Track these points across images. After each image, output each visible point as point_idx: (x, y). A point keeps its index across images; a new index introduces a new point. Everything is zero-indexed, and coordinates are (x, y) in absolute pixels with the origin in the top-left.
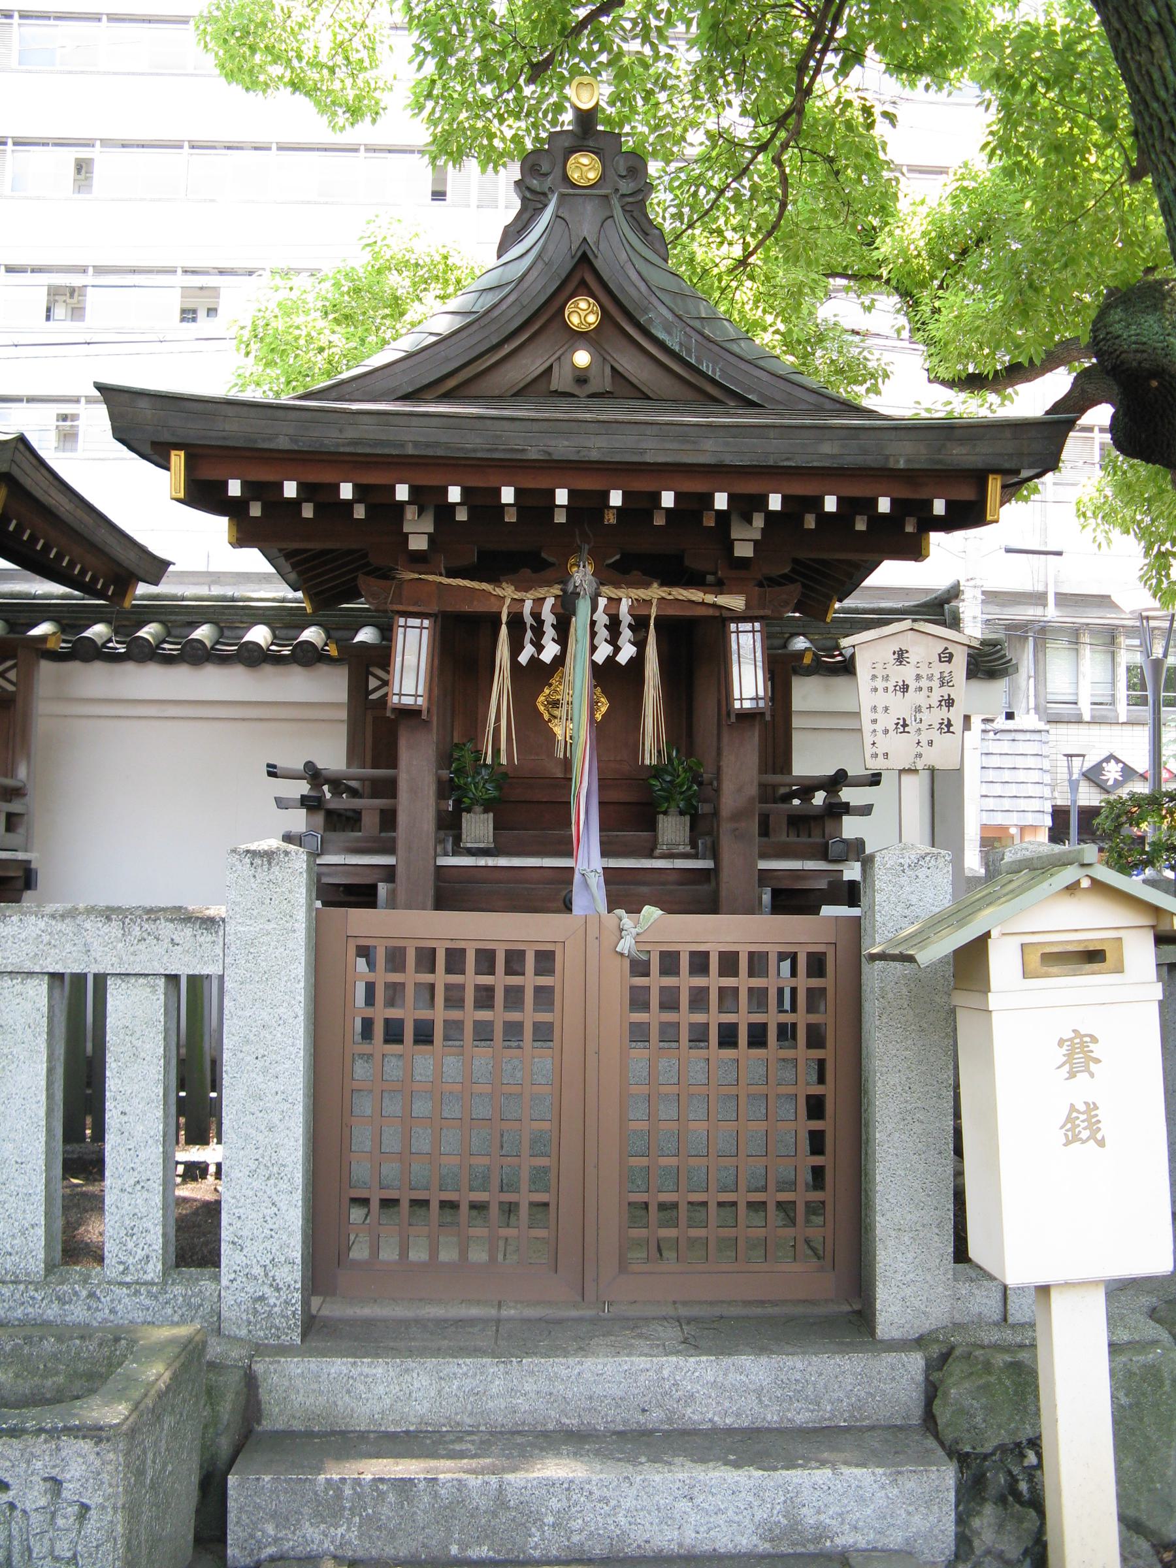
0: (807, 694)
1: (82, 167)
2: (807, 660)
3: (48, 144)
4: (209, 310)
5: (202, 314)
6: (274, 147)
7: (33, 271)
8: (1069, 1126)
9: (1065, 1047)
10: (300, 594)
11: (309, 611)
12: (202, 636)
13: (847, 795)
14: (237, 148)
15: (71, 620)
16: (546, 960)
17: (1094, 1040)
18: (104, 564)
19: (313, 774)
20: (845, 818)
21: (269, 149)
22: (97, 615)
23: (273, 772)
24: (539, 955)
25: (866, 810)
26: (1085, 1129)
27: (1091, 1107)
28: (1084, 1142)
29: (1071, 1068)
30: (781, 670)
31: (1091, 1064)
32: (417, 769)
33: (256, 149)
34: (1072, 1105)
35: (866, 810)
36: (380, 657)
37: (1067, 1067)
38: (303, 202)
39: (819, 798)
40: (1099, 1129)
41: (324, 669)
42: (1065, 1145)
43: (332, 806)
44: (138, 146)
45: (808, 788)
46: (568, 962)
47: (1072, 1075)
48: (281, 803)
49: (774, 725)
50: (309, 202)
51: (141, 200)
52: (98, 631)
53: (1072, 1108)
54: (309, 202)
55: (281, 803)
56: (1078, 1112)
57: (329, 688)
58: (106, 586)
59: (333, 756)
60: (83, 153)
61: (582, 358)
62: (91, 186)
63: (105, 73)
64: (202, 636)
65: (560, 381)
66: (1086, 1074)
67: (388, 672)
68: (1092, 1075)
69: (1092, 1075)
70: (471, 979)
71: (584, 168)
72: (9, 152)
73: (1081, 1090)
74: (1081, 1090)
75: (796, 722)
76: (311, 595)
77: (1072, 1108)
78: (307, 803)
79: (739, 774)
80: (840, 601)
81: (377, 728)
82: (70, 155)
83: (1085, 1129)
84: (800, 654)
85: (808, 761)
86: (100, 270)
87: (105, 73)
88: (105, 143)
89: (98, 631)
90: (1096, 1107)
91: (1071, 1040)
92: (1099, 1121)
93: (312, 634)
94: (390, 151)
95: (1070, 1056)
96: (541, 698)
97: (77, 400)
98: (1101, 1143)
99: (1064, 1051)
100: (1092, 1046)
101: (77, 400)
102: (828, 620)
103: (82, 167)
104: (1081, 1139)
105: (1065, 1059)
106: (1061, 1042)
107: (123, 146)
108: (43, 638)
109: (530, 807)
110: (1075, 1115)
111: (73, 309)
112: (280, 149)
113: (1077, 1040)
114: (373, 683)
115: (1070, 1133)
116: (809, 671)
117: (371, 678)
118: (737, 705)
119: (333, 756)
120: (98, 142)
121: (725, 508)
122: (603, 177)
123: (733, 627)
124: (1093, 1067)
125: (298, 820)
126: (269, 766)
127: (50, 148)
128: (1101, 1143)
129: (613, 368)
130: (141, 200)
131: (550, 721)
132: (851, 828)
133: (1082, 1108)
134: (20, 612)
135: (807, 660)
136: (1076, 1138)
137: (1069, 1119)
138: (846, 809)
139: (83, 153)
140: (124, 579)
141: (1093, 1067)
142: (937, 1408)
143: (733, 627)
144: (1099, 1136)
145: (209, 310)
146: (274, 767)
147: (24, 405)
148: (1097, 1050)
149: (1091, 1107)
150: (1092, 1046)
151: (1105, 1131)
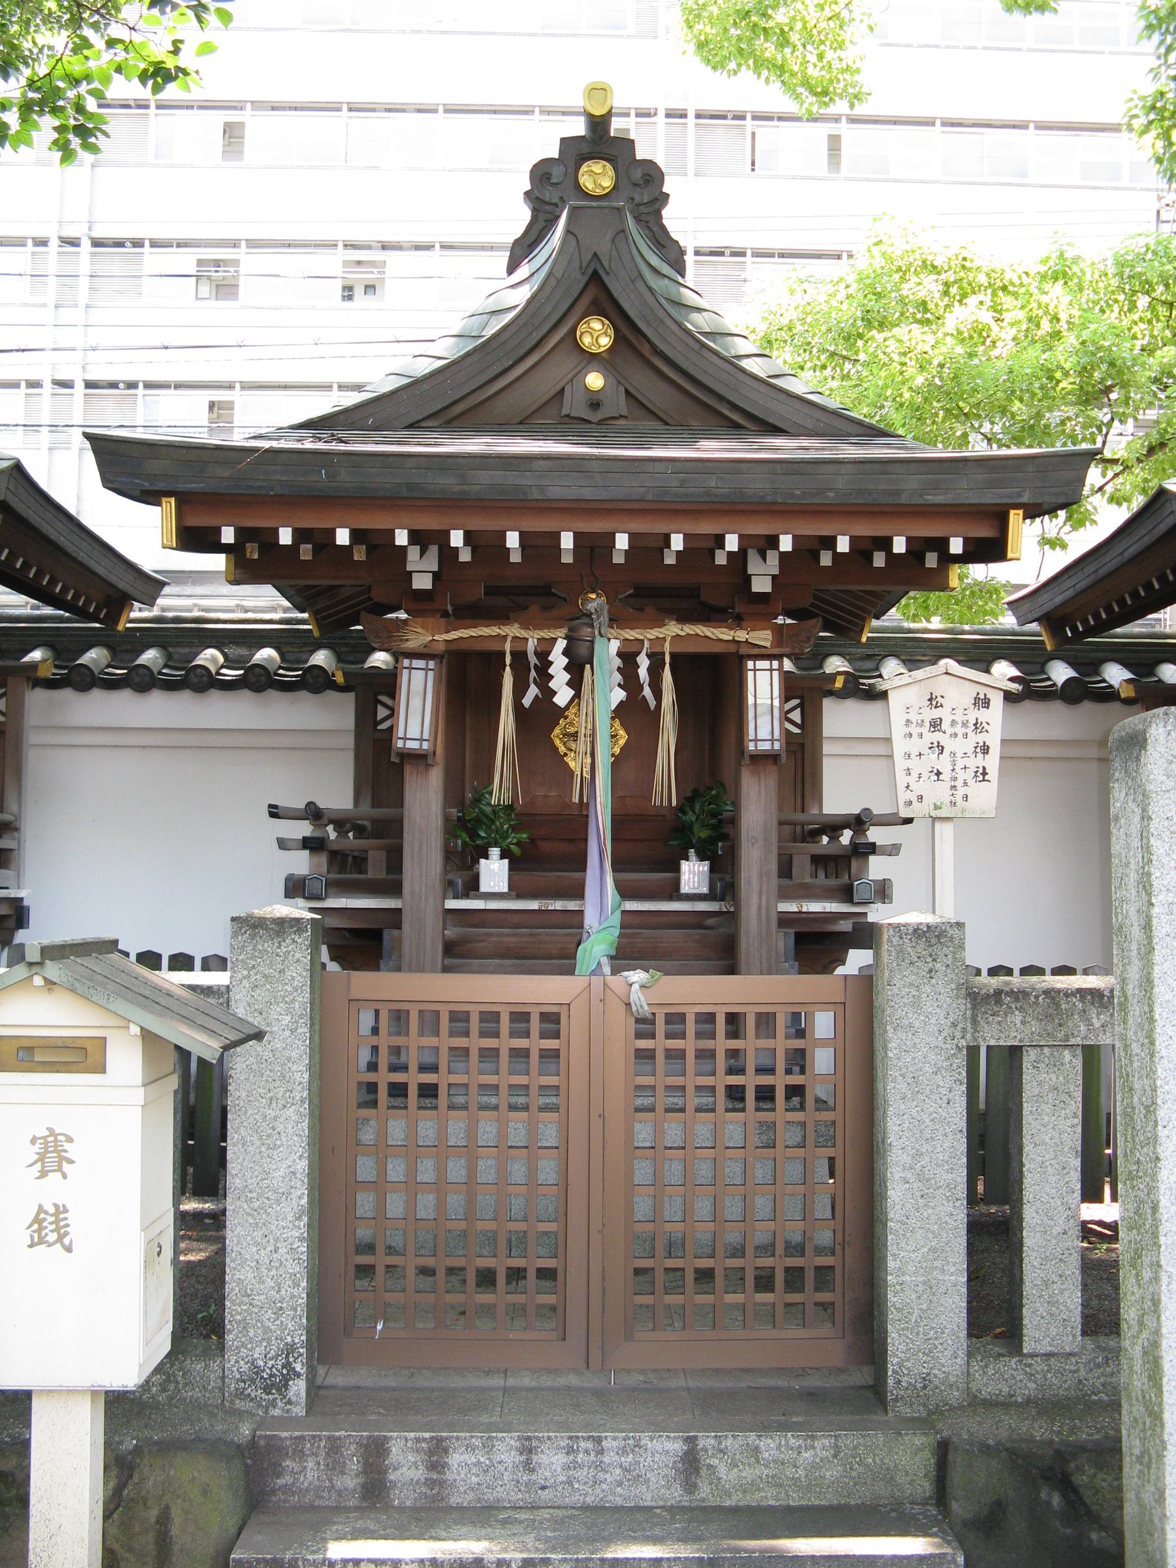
0: (839, 718)
1: (232, 134)
2: (839, 683)
3: (192, 107)
4: (366, 287)
5: (358, 292)
6: (441, 109)
7: (179, 246)
8: (36, 1226)
9: (38, 1145)
10: (305, 615)
11: (316, 634)
12: (181, 660)
13: (874, 835)
14: (397, 111)
15: (67, 647)
16: (552, 1021)
17: (70, 1140)
18: (90, 586)
19: (313, 813)
20: (872, 858)
21: (436, 111)
22: (89, 641)
23: (275, 812)
24: (545, 1017)
25: (893, 850)
26: (52, 1231)
27: (60, 1211)
28: (50, 1245)
29: (43, 1166)
30: (805, 692)
31: (64, 1163)
32: (425, 804)
33: (419, 111)
34: (40, 1207)
35: (893, 850)
36: (386, 685)
37: (38, 1166)
38: (474, 170)
39: (846, 837)
40: (67, 1234)
41: (331, 695)
42: (30, 1246)
43: (335, 847)
44: (290, 109)
45: (834, 827)
46: (574, 1026)
47: (43, 1174)
48: (283, 844)
49: (800, 759)
50: (480, 170)
51: (298, 167)
52: (94, 657)
53: (41, 1209)
54: (480, 170)
55: (283, 844)
56: (46, 1213)
57: (334, 715)
58: (98, 609)
59: (338, 794)
60: (233, 116)
61: (595, 381)
62: (242, 152)
63: (255, 29)
64: (181, 660)
65: (574, 405)
66: (59, 1174)
67: (393, 698)
68: (65, 1176)
69: (65, 1176)
70: (506, 1043)
71: (597, 177)
72: (152, 117)
73: (52, 1191)
74: (52, 1191)
75: (827, 748)
76: (319, 617)
77: (41, 1209)
78: (311, 844)
79: (757, 807)
80: (877, 618)
81: (380, 764)
82: (219, 118)
83: (52, 1231)
84: (833, 677)
85: (839, 795)
86: (253, 244)
87: (255, 29)
88: (257, 105)
89: (94, 657)
90: (66, 1211)
91: (45, 1138)
92: (67, 1225)
93: (321, 658)
94: (564, 113)
95: (42, 1158)
96: (557, 731)
97: (230, 386)
98: (69, 1249)
99: (37, 1148)
100: (67, 1146)
101: (230, 386)
102: (864, 640)
103: (232, 134)
104: (47, 1242)
105: (37, 1157)
106: (33, 1141)
107: (273, 109)
108: (34, 666)
109: (548, 850)
110: (42, 1216)
111: (217, 286)
112: (446, 111)
113: (51, 1139)
114: (382, 712)
115: (36, 1235)
116: (843, 694)
117: (380, 707)
118: (751, 746)
119: (338, 794)
120: (249, 105)
121: (348, 543)
122: (577, 186)
123: (750, 664)
124: (66, 1167)
125: (301, 863)
126: (270, 806)
127: (195, 111)
128: (69, 1249)
129: (626, 390)
130: (298, 167)
131: (566, 755)
132: (877, 867)
133: (52, 1210)
134: (30, 635)
135: (839, 683)
136: (42, 1241)
137: (37, 1220)
138: (872, 849)
139: (233, 116)
140: (118, 602)
141: (66, 1167)
142: (233, 1531)
143: (750, 664)
144: (66, 1241)
145: (366, 287)
146: (276, 807)
147: (172, 391)
148: (72, 1151)
149: (60, 1211)
150: (67, 1146)
151: (75, 1234)
